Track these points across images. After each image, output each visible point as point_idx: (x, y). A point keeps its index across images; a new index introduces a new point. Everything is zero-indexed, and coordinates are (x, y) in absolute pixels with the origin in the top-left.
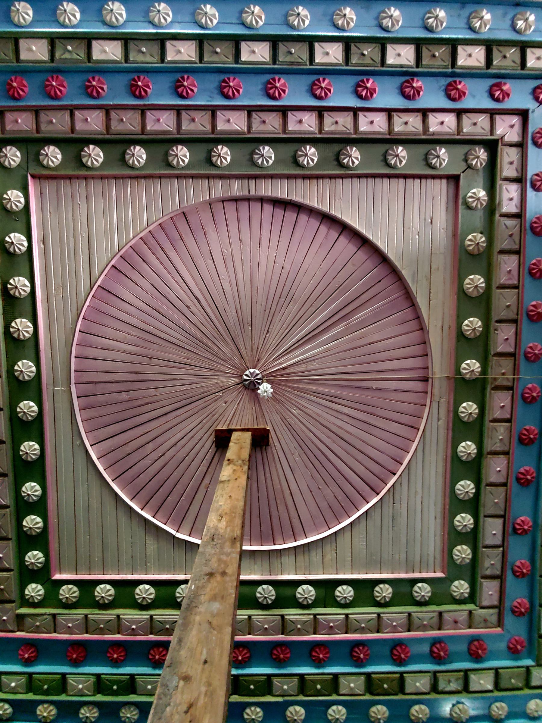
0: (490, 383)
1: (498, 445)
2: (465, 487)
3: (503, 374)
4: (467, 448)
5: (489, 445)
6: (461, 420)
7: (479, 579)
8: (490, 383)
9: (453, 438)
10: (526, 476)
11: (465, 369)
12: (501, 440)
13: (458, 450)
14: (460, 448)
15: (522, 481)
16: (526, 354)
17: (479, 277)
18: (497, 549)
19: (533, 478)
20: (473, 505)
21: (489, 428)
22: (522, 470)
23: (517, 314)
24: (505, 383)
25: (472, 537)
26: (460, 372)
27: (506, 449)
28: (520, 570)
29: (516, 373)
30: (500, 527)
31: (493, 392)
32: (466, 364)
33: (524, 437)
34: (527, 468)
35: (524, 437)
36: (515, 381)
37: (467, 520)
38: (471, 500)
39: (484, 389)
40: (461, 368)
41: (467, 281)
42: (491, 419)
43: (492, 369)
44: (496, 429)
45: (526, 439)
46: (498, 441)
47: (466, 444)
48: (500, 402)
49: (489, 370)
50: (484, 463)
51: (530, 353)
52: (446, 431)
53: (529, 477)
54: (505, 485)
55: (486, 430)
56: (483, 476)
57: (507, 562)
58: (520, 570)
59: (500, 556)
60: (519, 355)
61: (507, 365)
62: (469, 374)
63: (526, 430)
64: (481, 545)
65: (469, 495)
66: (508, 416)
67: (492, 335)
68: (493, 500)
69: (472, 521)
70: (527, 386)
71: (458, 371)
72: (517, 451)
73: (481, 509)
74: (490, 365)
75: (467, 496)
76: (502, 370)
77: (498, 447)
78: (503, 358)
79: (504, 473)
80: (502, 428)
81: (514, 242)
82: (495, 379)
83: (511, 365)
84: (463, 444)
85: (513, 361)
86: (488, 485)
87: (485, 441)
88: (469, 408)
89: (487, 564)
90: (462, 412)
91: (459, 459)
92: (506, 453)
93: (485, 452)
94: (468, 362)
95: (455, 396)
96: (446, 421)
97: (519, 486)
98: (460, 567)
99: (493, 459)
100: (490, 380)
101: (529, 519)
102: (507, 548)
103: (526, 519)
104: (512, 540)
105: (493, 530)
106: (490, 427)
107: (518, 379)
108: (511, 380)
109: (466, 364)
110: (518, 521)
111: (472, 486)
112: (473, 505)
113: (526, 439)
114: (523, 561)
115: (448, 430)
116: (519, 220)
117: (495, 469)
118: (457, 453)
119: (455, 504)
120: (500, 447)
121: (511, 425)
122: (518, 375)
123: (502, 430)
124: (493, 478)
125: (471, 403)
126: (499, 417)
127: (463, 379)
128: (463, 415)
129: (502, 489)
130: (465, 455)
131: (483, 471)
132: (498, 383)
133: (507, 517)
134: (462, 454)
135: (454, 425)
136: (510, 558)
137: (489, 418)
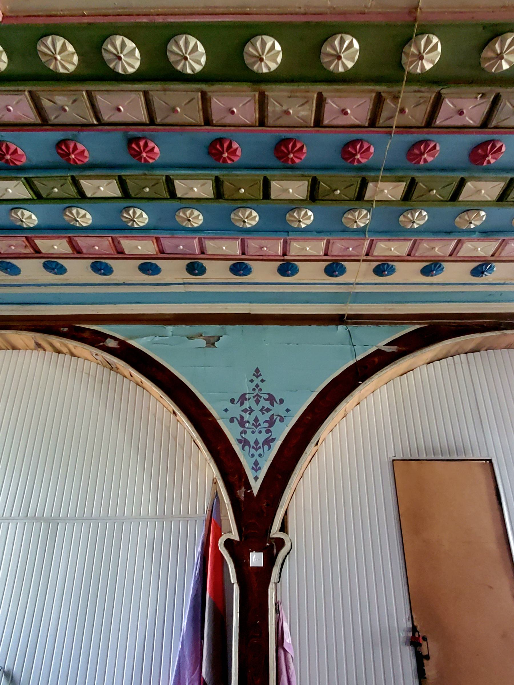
0: (390, 89)
1: (278, 108)
2: (193, 55)
3: (402, 111)
4: (270, 54)
5: (276, 94)
6: (249, 40)
7: (27, 88)
8: (390, 89)
9: (139, 26)
10: (227, 151)
11: (187, 43)
12: (287, 113)
13: (265, 37)
14: (270, 41)
15: (218, 147)
16: (426, 142)
17: (203, 60)
18: (92, 114)
19: (225, 161)
20: (159, 71)
21: (307, 92)
22: (235, 145)
23: (495, 127)
24: (384, 114)
25: (97, 72)
26: (423, 33)
27: (270, 121)
28: (71, 150)
29: (398, 129)
30: (134, 119)
31: (374, 95)
32: (196, 45)
33: (290, 146)
34: (238, 153)
35: (290, 146)
36: (389, 129)
37: (130, 61)
38: (246, 67)
39: (378, 80)
40: (431, 36)
41: (193, 41)
42: (325, 94)
43: (415, 92)
44: (307, 102)
45: (287, 148)
46: (285, 108)
47: (279, 52)
48: (351, 107)
49: (416, 88)
50: (245, 86)
51: (222, 146)
52: (302, 10)
53: (226, 155)
54: (208, 121)
55: (303, 87)
56: (217, 87)
57: (79, 131)
58: (71, 150)
59: (85, 121)
60: (428, 133)
61: (416, 114)
62: (416, 52)
63: (302, 148)
64: (34, 88)
65: (178, 62)
66: (159, 120)
67: (476, 89)
68: (179, 103)
69: (131, 70)
70: (372, 146)
71: (425, 30)
72: (267, 137)
73: (158, 86)
74: (423, 89)
75: (253, 60)
76: (411, 106)
77: (274, 108)
78: (429, 108)
79: (229, 119)
80: (306, 113)
81: (279, 118)
82: (396, 98)
83: (413, 122)
84: (278, 47)
85: (419, 125)
86: (204, 94)
87: (283, 87)
88: (348, 52)
89: (61, 100)
90: (342, 41)
91: (248, 39)
92: (262, 122)
93: (263, 87)
94: (201, 49)
95: (378, 27)
96: (321, 10)
97: (208, 143)
98: (163, 51)
99: (253, 101)
100: (396, 89)
101: (24, 159)
102: (98, 130)
103: (156, 154)
104: (117, 137)
105: (126, 106)
106: (309, 94)
107: (390, 133)
108: (388, 123)
109: (196, 45)
110: (151, 144)
111: (198, 68)
112: (159, 71)
113: (288, 149)
114: (86, 154)
115: (305, 14)
116: (367, 125)
117: (235, 105)
118: (261, 34)
119: (156, 37)
120: (274, 111)
121: (311, 127)
122: (395, 133)
123: (302, 112)
124: (218, 103)
125: (279, 59)
126: (327, 108)
127: (408, 40)
128: (337, 42)
129: (200, 118)
130: (257, 51)
131: (228, 86)
132: (389, 104)
133: (100, 127)
134: (258, 44)
135: (318, 24)
136: (83, 135)
137: (327, 91)
